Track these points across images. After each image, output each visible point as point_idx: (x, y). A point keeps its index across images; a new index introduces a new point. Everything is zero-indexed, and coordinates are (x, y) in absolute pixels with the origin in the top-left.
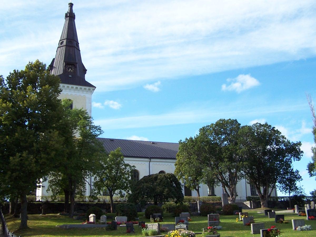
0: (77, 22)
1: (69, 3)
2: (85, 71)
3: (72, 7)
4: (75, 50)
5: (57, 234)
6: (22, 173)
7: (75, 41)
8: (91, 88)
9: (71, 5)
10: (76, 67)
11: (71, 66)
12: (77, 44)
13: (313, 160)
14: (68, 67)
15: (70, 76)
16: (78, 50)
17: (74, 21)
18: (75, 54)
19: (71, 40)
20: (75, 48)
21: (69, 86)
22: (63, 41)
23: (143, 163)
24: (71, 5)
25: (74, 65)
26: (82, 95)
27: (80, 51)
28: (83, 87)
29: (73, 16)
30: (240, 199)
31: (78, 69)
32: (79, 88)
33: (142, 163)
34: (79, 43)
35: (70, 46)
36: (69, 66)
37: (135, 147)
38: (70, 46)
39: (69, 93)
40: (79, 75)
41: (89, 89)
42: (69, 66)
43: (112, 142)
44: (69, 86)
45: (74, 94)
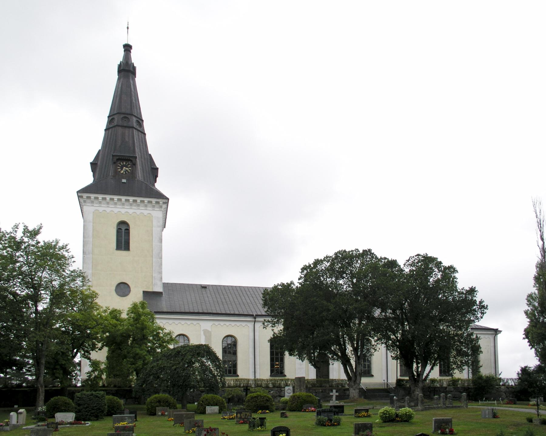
0: (140, 80)
1: (124, 43)
2: (154, 171)
3: (130, 52)
4: (133, 133)
5: (340, 382)
6: (90, 333)
7: (133, 115)
8: (161, 201)
9: (128, 48)
10: (134, 164)
11: (126, 163)
12: (140, 122)
13: (528, 318)
14: (121, 164)
15: (124, 181)
16: (140, 133)
17: (135, 80)
18: (134, 141)
19: (128, 114)
20: (134, 130)
21: (106, 197)
22: (113, 117)
23: (244, 324)
24: (128, 48)
25: (131, 161)
26: (146, 212)
27: (145, 134)
28: (154, 200)
29: (131, 69)
30: (383, 382)
31: (139, 167)
32: (108, 199)
33: (236, 325)
34: (143, 121)
35: (126, 127)
36: (121, 163)
37: (239, 298)
38: (126, 127)
39: (123, 211)
40: (141, 178)
41: (157, 203)
42: (121, 163)
43: (203, 290)
44: (106, 197)
45: (131, 211)
